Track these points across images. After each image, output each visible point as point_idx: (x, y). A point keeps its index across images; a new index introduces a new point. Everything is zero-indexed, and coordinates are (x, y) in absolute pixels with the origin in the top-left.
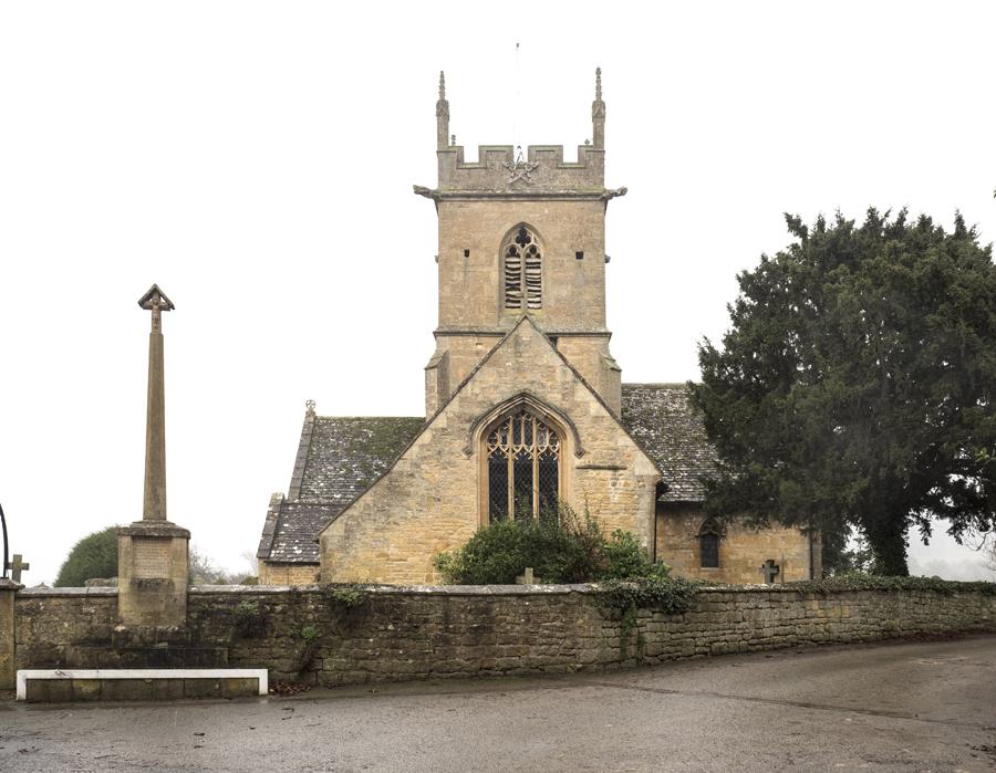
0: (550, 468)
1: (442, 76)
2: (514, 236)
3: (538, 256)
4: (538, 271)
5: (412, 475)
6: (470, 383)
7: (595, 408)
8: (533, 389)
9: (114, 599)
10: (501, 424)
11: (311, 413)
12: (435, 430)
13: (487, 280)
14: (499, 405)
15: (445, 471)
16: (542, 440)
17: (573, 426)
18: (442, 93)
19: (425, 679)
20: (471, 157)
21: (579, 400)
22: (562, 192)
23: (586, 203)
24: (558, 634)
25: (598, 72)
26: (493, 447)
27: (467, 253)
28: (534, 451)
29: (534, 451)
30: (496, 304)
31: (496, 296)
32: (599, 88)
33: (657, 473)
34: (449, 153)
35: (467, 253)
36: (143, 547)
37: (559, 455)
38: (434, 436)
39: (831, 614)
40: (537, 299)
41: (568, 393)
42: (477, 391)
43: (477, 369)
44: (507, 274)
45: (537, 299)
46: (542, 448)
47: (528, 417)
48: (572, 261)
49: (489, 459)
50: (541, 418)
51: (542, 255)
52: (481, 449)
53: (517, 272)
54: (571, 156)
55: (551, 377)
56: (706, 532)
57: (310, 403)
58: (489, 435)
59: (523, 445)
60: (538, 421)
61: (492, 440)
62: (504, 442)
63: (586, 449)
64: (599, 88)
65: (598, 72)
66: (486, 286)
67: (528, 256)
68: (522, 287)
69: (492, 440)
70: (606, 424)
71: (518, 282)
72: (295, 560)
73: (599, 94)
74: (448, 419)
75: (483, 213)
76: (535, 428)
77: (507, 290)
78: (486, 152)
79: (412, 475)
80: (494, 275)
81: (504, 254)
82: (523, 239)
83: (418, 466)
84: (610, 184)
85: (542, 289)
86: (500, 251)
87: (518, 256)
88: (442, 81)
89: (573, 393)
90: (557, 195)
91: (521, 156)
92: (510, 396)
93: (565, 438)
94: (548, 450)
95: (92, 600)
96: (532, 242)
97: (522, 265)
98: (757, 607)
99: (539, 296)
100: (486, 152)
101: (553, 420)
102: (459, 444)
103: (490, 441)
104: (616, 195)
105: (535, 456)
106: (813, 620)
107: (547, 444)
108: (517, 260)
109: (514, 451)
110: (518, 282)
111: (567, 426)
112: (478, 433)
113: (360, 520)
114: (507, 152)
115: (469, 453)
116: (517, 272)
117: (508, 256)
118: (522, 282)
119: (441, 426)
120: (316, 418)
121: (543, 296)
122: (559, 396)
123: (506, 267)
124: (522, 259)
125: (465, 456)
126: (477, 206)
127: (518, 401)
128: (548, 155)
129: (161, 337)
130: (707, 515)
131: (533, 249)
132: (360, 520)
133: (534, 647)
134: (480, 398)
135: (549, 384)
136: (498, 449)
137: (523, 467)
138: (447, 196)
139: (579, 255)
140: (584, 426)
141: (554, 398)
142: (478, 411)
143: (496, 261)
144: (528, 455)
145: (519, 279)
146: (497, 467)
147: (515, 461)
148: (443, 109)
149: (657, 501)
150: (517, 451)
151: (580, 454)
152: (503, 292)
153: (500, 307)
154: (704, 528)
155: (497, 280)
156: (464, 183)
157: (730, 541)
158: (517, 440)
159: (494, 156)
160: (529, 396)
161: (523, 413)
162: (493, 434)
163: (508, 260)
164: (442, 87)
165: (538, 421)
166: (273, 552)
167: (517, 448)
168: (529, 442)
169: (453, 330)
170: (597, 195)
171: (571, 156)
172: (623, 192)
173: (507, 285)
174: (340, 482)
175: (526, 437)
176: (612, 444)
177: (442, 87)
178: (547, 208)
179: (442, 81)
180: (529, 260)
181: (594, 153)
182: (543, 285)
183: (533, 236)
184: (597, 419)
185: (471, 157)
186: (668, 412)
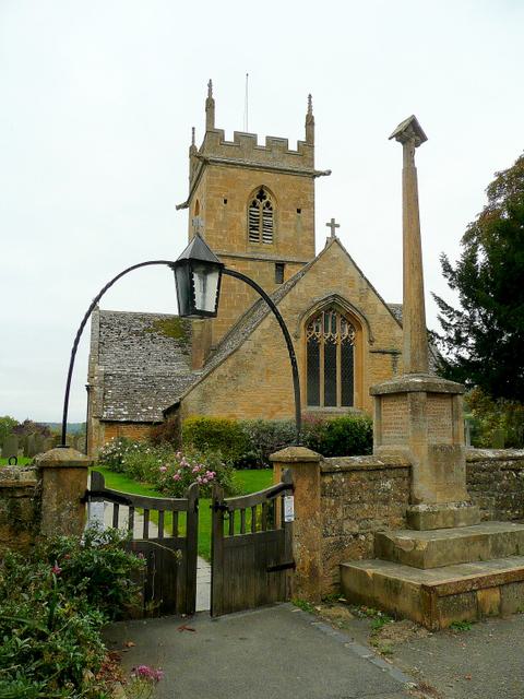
1: (210, 85)
2: (256, 193)
3: (271, 209)
5: (255, 353)
10: (316, 317)
13: (239, 220)
16: (343, 329)
17: (367, 322)
20: (229, 138)
25: (310, 97)
27: (225, 202)
28: (339, 337)
34: (213, 134)
48: (293, 215)
54: (293, 147)
55: (352, 285)
58: (309, 326)
65: (310, 97)
66: (238, 224)
68: (261, 228)
72: (124, 419)
73: (310, 109)
76: (339, 321)
78: (237, 135)
79: (255, 353)
80: (244, 219)
82: (261, 196)
84: (318, 167)
90: (286, 171)
91: (261, 142)
94: (314, 335)
100: (237, 135)
103: (309, 329)
104: (324, 174)
111: (363, 321)
112: (303, 324)
114: (252, 138)
118: (261, 225)
122: (358, 299)
127: (331, 300)
128: (276, 144)
129: (414, 171)
131: (268, 204)
136: (314, 335)
139: (299, 211)
142: (304, 306)
151: (371, 342)
156: (213, 159)
158: (326, 330)
159: (245, 140)
161: (330, 310)
168: (334, 331)
171: (293, 147)
178: (279, 178)
181: (308, 145)
182: (274, 228)
183: (268, 195)
185: (229, 138)
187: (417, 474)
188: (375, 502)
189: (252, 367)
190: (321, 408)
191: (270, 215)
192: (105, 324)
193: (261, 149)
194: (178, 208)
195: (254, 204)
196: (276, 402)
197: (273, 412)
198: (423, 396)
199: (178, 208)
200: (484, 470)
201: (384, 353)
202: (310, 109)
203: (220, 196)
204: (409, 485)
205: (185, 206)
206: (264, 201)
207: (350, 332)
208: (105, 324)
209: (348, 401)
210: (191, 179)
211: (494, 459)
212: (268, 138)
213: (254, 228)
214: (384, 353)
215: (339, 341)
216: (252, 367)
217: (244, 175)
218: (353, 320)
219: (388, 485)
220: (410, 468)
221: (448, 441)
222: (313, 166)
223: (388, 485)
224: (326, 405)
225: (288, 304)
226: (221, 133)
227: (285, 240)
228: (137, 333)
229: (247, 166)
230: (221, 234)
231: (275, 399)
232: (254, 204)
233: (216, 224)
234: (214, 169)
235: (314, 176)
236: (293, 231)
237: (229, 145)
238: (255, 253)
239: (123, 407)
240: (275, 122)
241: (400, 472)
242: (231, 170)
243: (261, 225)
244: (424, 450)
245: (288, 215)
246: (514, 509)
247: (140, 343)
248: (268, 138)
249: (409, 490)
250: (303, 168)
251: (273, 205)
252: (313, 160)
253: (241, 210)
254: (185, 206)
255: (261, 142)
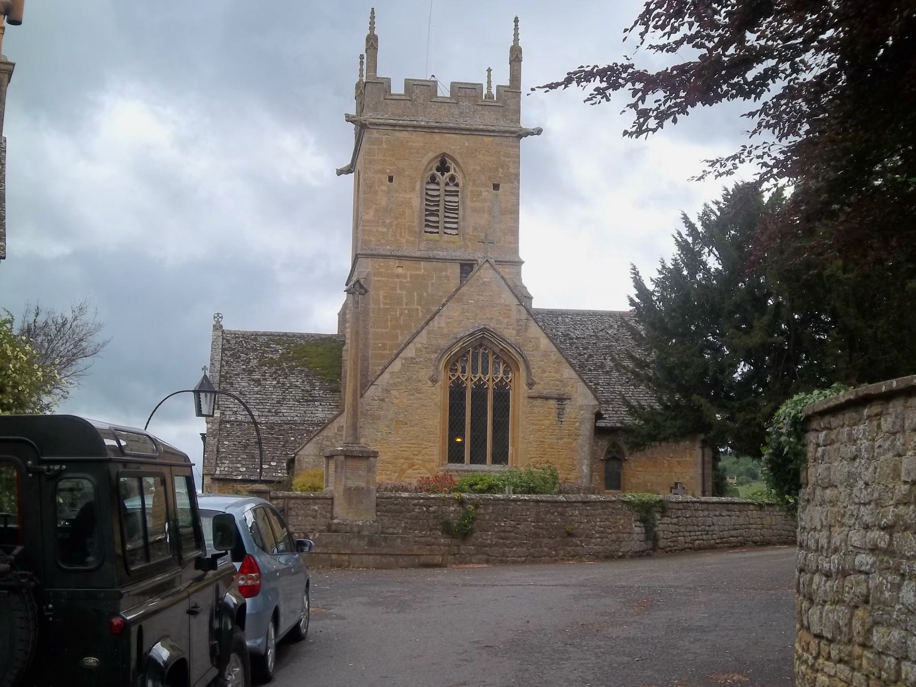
0: (502, 397)
2: (437, 164)
3: (457, 185)
4: (455, 199)
5: (383, 400)
6: (436, 317)
7: (544, 342)
8: (492, 325)
9: (330, 502)
10: (462, 355)
11: (218, 327)
12: (406, 359)
14: (462, 338)
15: (411, 397)
16: (496, 370)
17: (525, 361)
18: (372, 28)
19: (523, 562)
20: (398, 88)
21: (532, 336)
22: (481, 127)
23: (503, 139)
24: (610, 531)
26: (453, 375)
27: (391, 179)
28: (490, 381)
29: (490, 381)
30: (417, 229)
31: (417, 221)
32: (516, 35)
33: (596, 403)
35: (391, 179)
36: (350, 463)
37: (512, 384)
38: (403, 365)
39: (765, 523)
40: (455, 226)
41: (522, 329)
42: (443, 325)
43: (444, 305)
44: (427, 200)
45: (455, 226)
46: (497, 377)
47: (485, 349)
48: (487, 193)
49: (450, 387)
50: (497, 350)
51: (461, 184)
52: (443, 377)
53: (437, 199)
56: (609, 456)
57: (218, 317)
58: (451, 366)
59: (479, 375)
60: (494, 353)
61: (454, 370)
62: (464, 371)
63: (536, 379)
64: (516, 35)
65: (516, 20)
66: (408, 211)
67: (447, 184)
68: (441, 213)
69: (454, 370)
70: (553, 358)
71: (437, 213)
72: (240, 477)
73: (516, 40)
74: (416, 349)
75: (407, 142)
76: (491, 359)
77: (426, 215)
78: (410, 85)
79: (383, 400)
80: (416, 201)
81: (425, 181)
83: (388, 391)
85: (461, 217)
86: (422, 178)
87: (438, 184)
88: (372, 18)
89: (527, 328)
91: (444, 91)
92: (472, 331)
93: (518, 369)
95: (317, 501)
96: (452, 172)
97: (442, 192)
98: (721, 515)
99: (457, 223)
100: (410, 85)
101: (508, 354)
102: (425, 374)
103: (451, 370)
104: (532, 134)
105: (491, 385)
106: (754, 526)
107: (501, 375)
108: (437, 187)
109: (472, 380)
110: (437, 213)
111: (521, 360)
113: (333, 441)
114: (430, 87)
115: (434, 381)
116: (437, 199)
117: (428, 183)
118: (441, 208)
119: (410, 355)
120: (223, 332)
121: (461, 224)
122: (514, 332)
123: (427, 194)
124: (442, 185)
125: (430, 383)
126: (404, 135)
127: (479, 335)
130: (615, 444)
131: (452, 178)
132: (333, 441)
133: (593, 540)
134: (445, 331)
135: (506, 320)
137: (479, 393)
138: (375, 124)
139: (496, 187)
140: (536, 362)
141: (510, 334)
142: (444, 343)
143: (418, 187)
144: (484, 384)
145: (438, 205)
146: (456, 394)
147: (473, 389)
148: (372, 42)
149: (596, 426)
150: (475, 380)
151: (531, 385)
152: (424, 218)
153: (420, 232)
154: (609, 452)
155: (418, 206)
157: (632, 464)
158: (474, 370)
160: (488, 331)
161: (481, 345)
162: (454, 365)
163: (428, 187)
164: (372, 23)
165: (494, 353)
166: (218, 469)
167: (475, 377)
168: (485, 372)
169: (374, 252)
170: (513, 132)
172: (539, 132)
173: (427, 210)
174: (257, 399)
175: (483, 367)
176: (558, 376)
177: (372, 23)
179: (372, 18)
180: (448, 188)
182: (461, 212)
183: (452, 166)
184: (546, 355)
185: (398, 88)
186: (571, 339)
187: (336, 502)
188: (306, 516)
189: (379, 418)
190: (467, 466)
191: (455, 194)
192: (230, 349)
193: (443, 102)
194: (340, 172)
195: (433, 179)
196: (407, 459)
197: (403, 471)
198: (342, 458)
199: (340, 172)
200: (396, 505)
201: (547, 398)
202: (516, 40)
203: (382, 172)
204: (332, 509)
205: (348, 170)
206: (446, 174)
207: (505, 372)
208: (230, 349)
209: (501, 457)
210: (356, 134)
211: (407, 498)
212: (453, 85)
213: (432, 213)
214: (547, 398)
215: (491, 385)
216: (379, 418)
217: (416, 140)
218: (508, 359)
219: (316, 508)
220: (332, 499)
221: (363, 485)
222: (518, 121)
223: (316, 508)
224: (473, 461)
225: (425, 342)
226: (384, 85)
227: (475, 229)
228: (271, 363)
229: (424, 127)
230: (384, 224)
231: (406, 454)
232: (433, 179)
233: (377, 211)
234: (375, 134)
235: (520, 137)
236: (486, 216)
237: (397, 99)
238: (432, 250)
239: (239, 462)
240: (461, 59)
241: (325, 501)
242: (398, 134)
243: (441, 208)
244: (341, 489)
245: (480, 194)
246: (421, 530)
247: (274, 375)
248: (453, 85)
249: (332, 513)
250: (503, 125)
251: (459, 179)
252: (518, 111)
253: (413, 189)
254: (348, 170)
255: (444, 91)
